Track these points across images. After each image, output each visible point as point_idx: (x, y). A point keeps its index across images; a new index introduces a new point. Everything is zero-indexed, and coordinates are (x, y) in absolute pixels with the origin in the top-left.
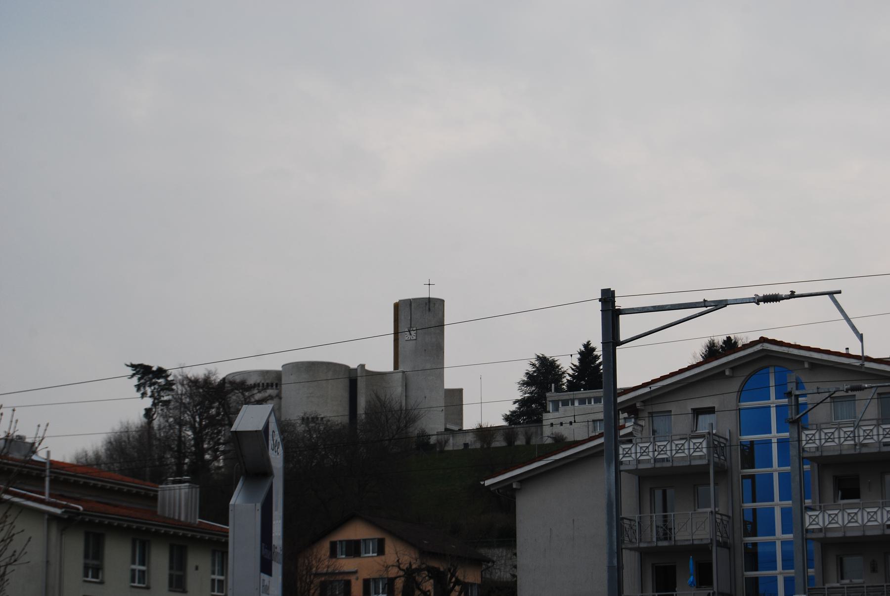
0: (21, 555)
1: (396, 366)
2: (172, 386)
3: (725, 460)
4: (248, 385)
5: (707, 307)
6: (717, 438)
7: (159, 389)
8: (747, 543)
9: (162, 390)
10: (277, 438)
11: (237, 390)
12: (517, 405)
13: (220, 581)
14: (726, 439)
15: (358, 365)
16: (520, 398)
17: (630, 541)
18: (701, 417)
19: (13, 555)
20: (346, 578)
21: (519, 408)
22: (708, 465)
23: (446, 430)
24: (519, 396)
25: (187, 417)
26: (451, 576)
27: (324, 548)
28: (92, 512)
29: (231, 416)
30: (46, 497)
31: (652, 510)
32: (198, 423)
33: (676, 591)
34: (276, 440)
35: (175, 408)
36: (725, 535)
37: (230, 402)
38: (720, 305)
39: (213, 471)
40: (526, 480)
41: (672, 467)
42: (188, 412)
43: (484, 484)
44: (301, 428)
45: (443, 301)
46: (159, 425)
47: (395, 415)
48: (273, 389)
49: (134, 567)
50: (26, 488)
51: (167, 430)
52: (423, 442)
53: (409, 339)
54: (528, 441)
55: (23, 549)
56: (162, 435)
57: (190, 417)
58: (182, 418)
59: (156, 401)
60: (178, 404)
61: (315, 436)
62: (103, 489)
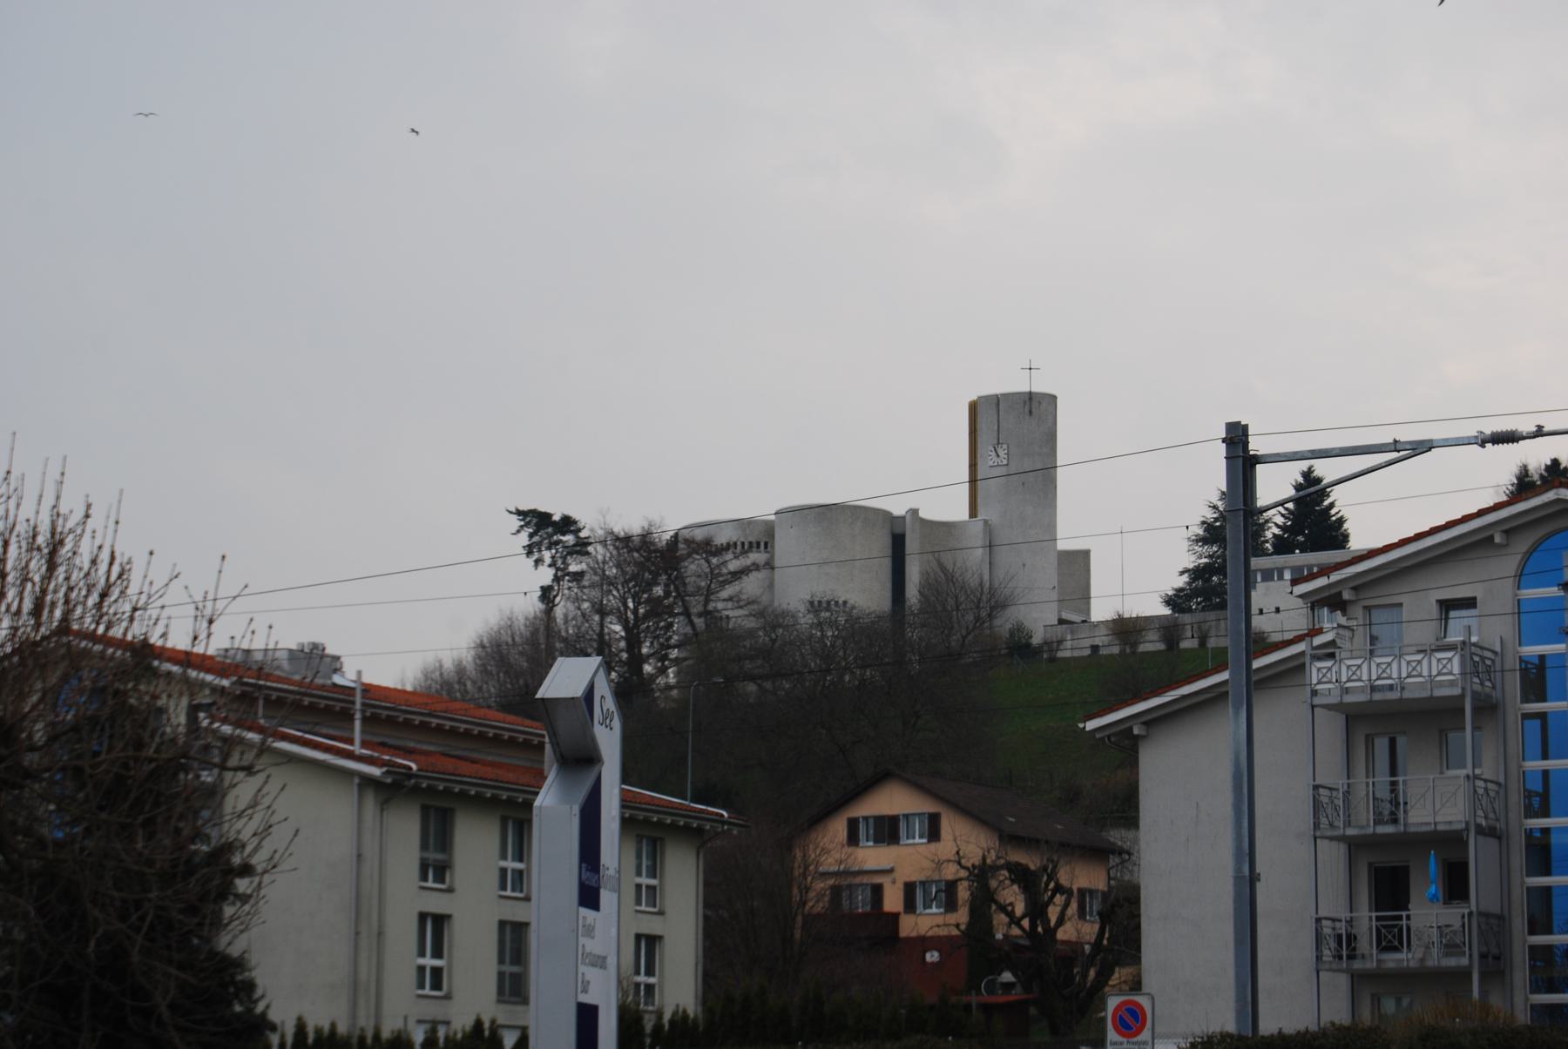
0: (283, 859)
1: (973, 512)
2: (586, 547)
3: (1494, 687)
4: (716, 545)
5: (1399, 451)
6: (1479, 651)
7: (565, 553)
8: (1531, 829)
9: (570, 554)
10: (610, 704)
11: (698, 554)
12: (1185, 578)
13: (651, 889)
14: (1495, 653)
15: (907, 510)
16: (1191, 566)
17: (1331, 825)
18: (1452, 614)
19: (272, 858)
20: (877, 880)
21: (1189, 584)
22: (1462, 696)
23: (1061, 622)
24: (1190, 561)
25: (612, 601)
26: (1047, 880)
27: (837, 828)
28: (432, 772)
29: (687, 598)
30: (356, 748)
31: (1370, 771)
32: (631, 610)
33: (1409, 910)
34: (608, 710)
35: (592, 586)
36: (1492, 815)
37: (685, 575)
38: (1421, 448)
39: (658, 694)
40: (1154, 721)
41: (1401, 700)
42: (615, 593)
43: (1085, 727)
44: (806, 620)
45: (1053, 398)
46: (566, 616)
47: (972, 596)
48: (760, 552)
49: (503, 864)
50: (324, 731)
51: (579, 624)
52: (1020, 647)
53: (996, 464)
54: (1203, 643)
55: (287, 849)
56: (571, 632)
57: (617, 601)
58: (605, 602)
59: (559, 574)
60: (597, 578)
61: (830, 634)
62: (453, 732)
